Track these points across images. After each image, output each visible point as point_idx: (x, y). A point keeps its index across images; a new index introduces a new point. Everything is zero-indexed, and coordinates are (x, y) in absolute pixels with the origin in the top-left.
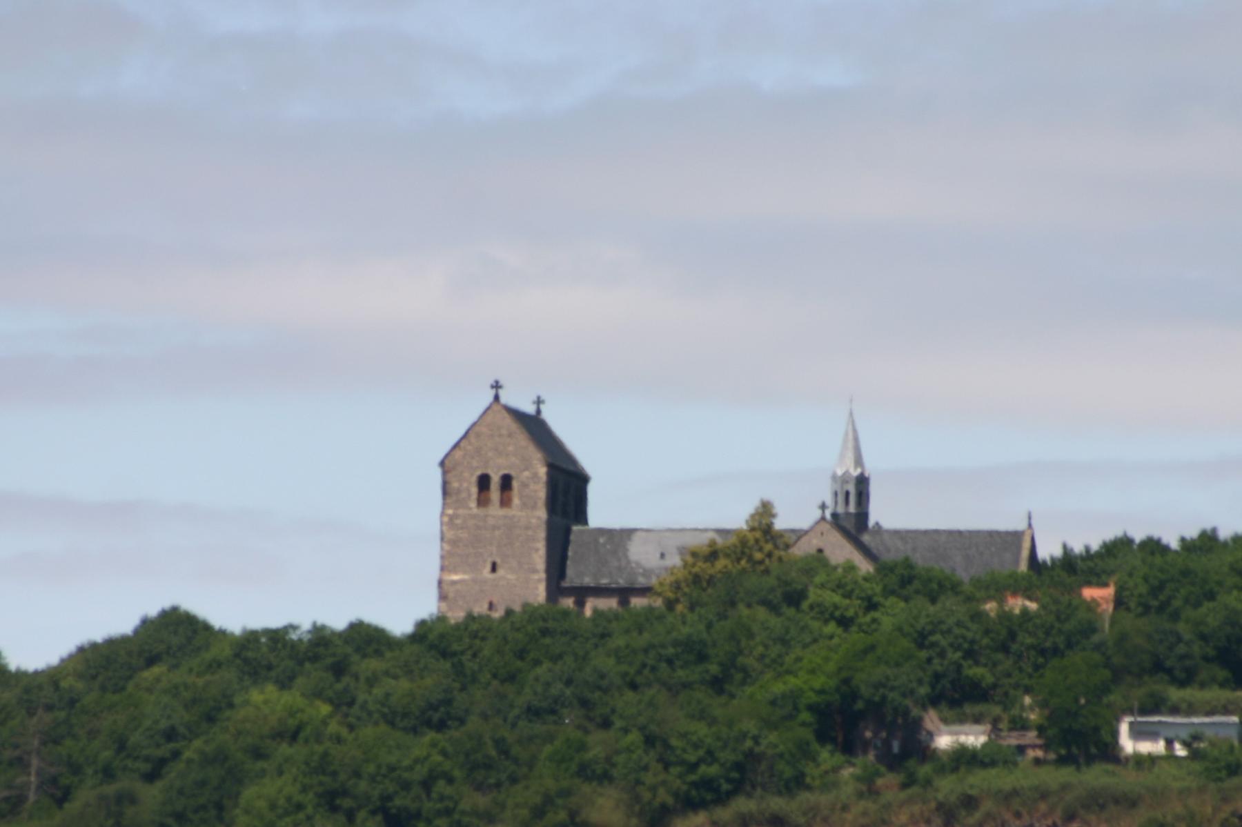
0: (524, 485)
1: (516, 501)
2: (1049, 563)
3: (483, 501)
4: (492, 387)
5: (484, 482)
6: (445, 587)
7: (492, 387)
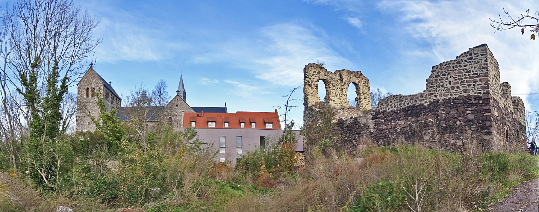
3: (87, 96)
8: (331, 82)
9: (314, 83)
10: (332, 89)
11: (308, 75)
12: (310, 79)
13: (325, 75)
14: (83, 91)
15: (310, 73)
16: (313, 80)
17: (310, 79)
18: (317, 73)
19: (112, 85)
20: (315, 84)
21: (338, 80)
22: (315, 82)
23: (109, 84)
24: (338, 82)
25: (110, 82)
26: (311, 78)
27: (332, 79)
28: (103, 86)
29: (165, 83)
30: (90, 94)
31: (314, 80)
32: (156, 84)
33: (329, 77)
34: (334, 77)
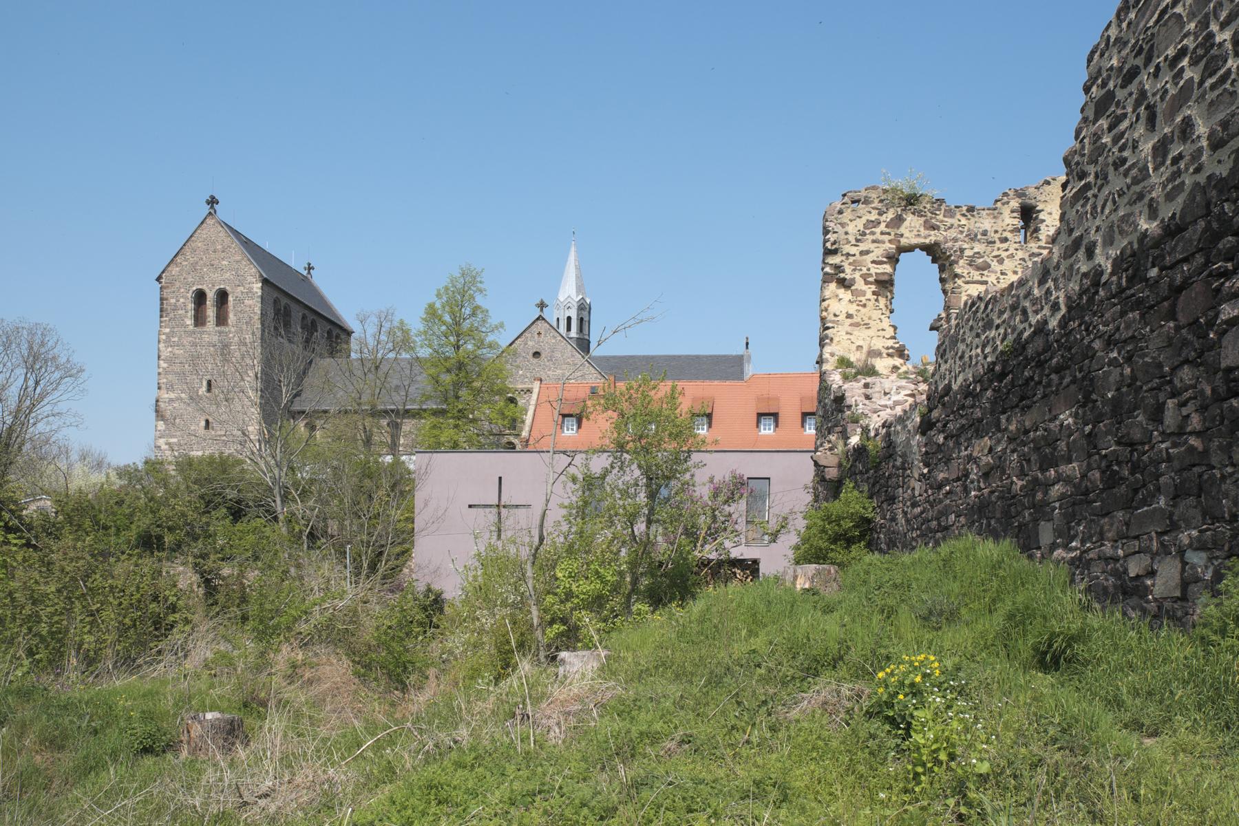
0: (239, 301)
1: (232, 318)
2: (140, 466)
3: (199, 320)
4: (538, 306)
5: (200, 297)
6: (162, 405)
7: (538, 306)
8: (968, 253)
9: (865, 270)
10: (967, 283)
11: (835, 243)
12: (844, 258)
13: (934, 228)
14: (182, 300)
15: (846, 233)
16: (864, 257)
17: (848, 255)
18: (887, 226)
19: (317, 279)
20: (871, 275)
21: (1006, 234)
22: (870, 265)
23: (305, 273)
24: (1005, 245)
25: (310, 268)
26: (853, 250)
27: (973, 238)
28: (260, 285)
29: (479, 279)
30: (211, 312)
31: (869, 258)
32: (444, 282)
33: (952, 233)
34: (986, 223)
